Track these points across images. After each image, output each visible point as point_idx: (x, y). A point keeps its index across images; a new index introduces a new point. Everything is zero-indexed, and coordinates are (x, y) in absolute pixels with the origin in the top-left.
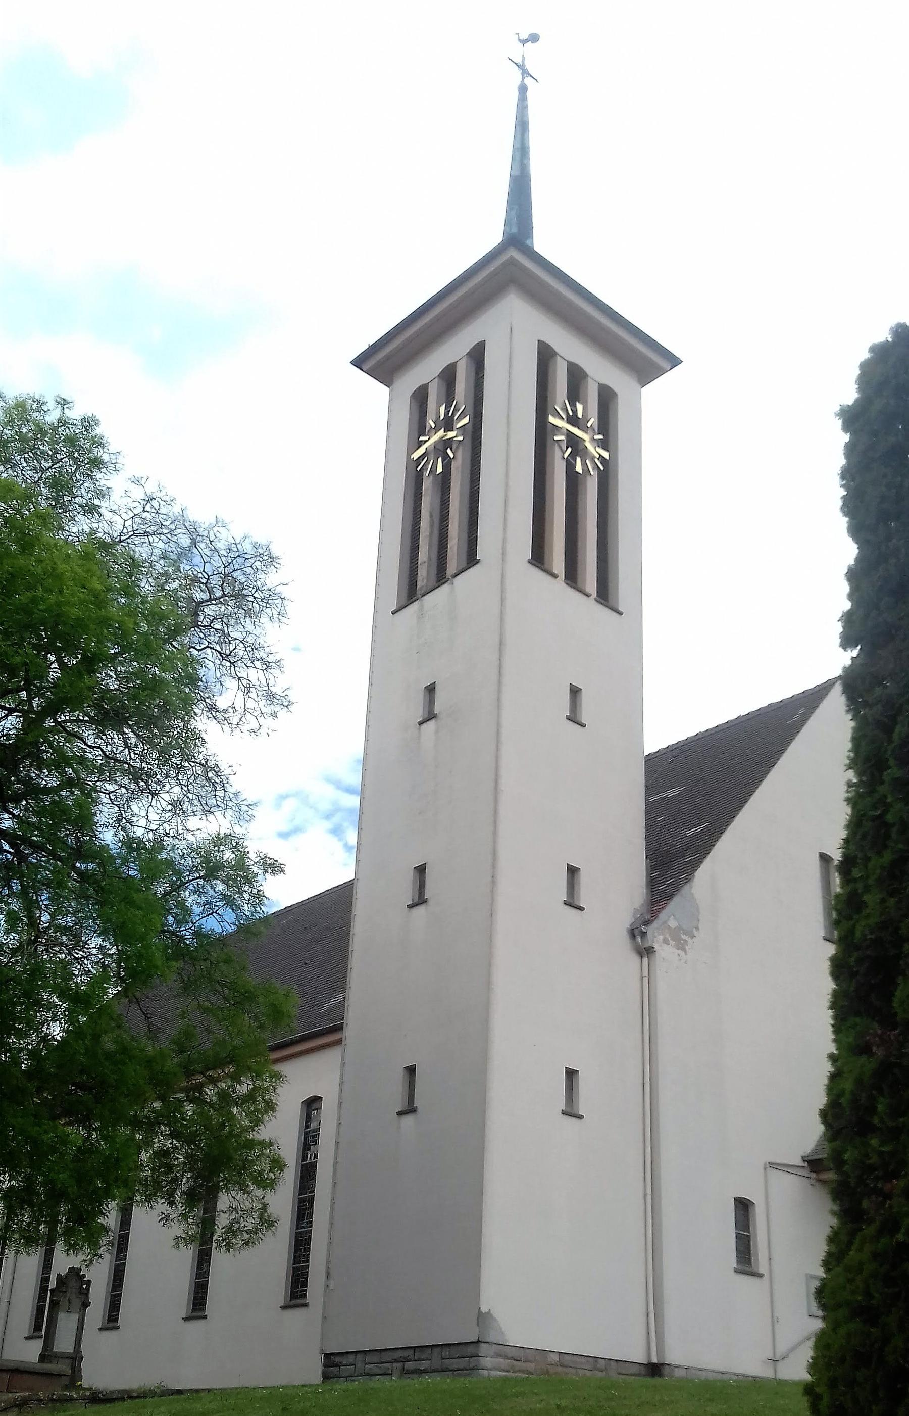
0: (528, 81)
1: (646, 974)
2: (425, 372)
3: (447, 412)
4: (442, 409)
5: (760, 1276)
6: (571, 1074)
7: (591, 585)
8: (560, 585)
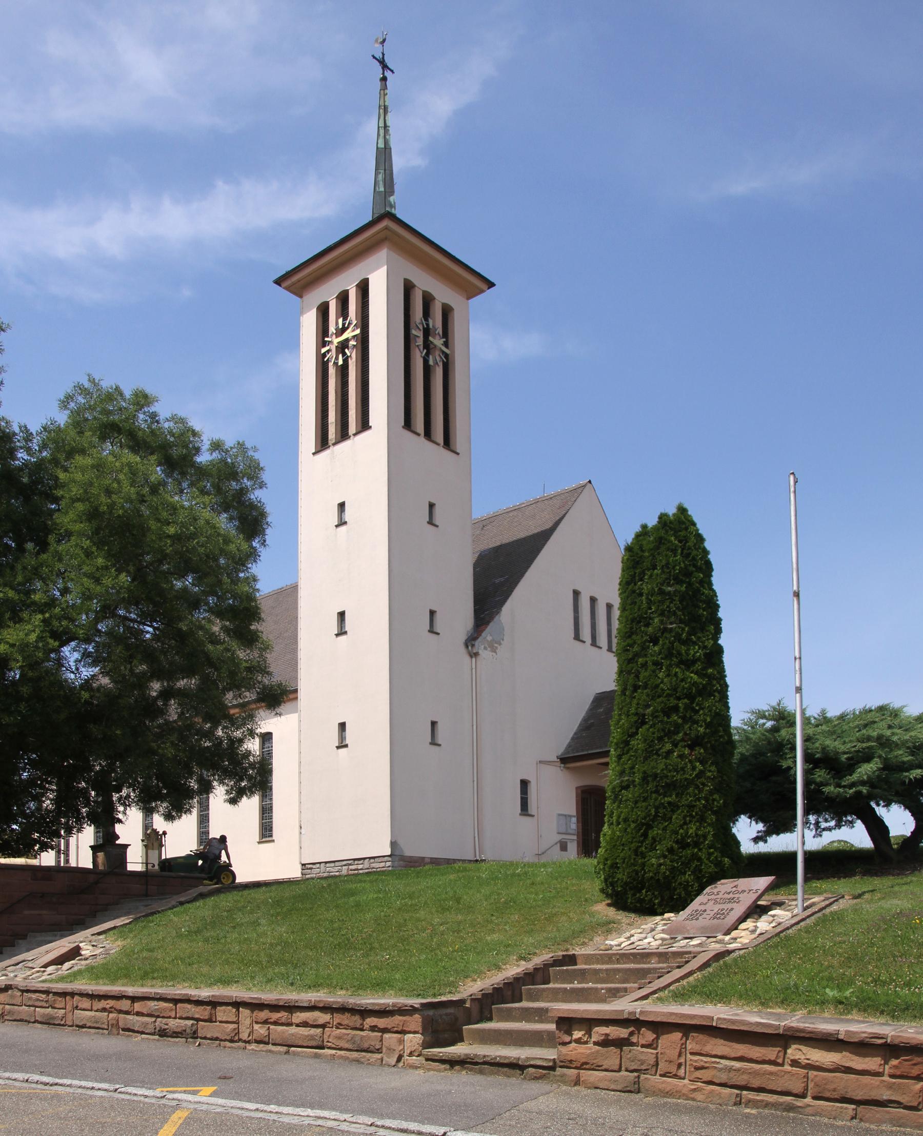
0: (388, 74)
1: (474, 666)
2: (328, 292)
3: (344, 324)
4: (340, 321)
5: (533, 816)
6: (434, 724)
7: (440, 438)
8: (422, 439)
